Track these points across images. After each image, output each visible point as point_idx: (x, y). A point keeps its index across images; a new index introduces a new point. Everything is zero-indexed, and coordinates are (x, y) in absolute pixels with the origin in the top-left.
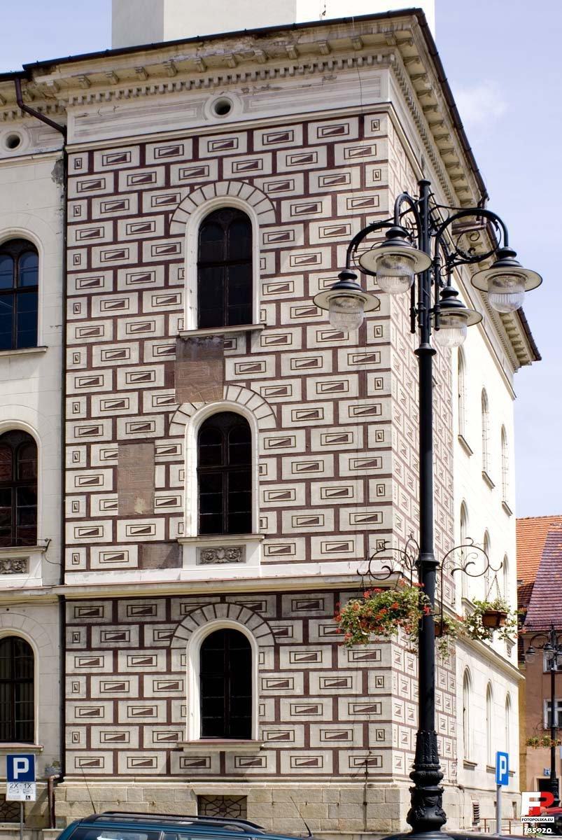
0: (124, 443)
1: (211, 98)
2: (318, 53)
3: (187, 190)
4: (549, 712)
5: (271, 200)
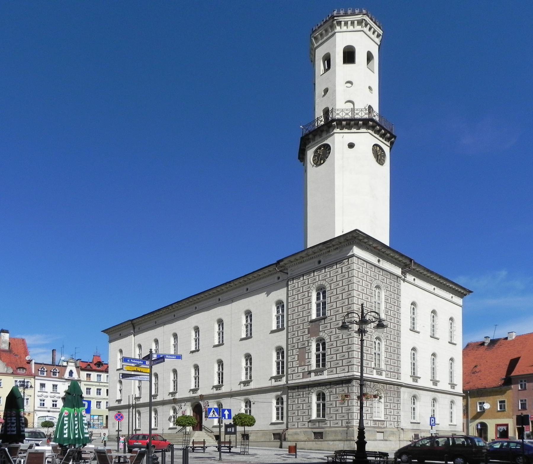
0: (299, 349)
1: (316, 260)
2: (337, 244)
4: (316, 375)
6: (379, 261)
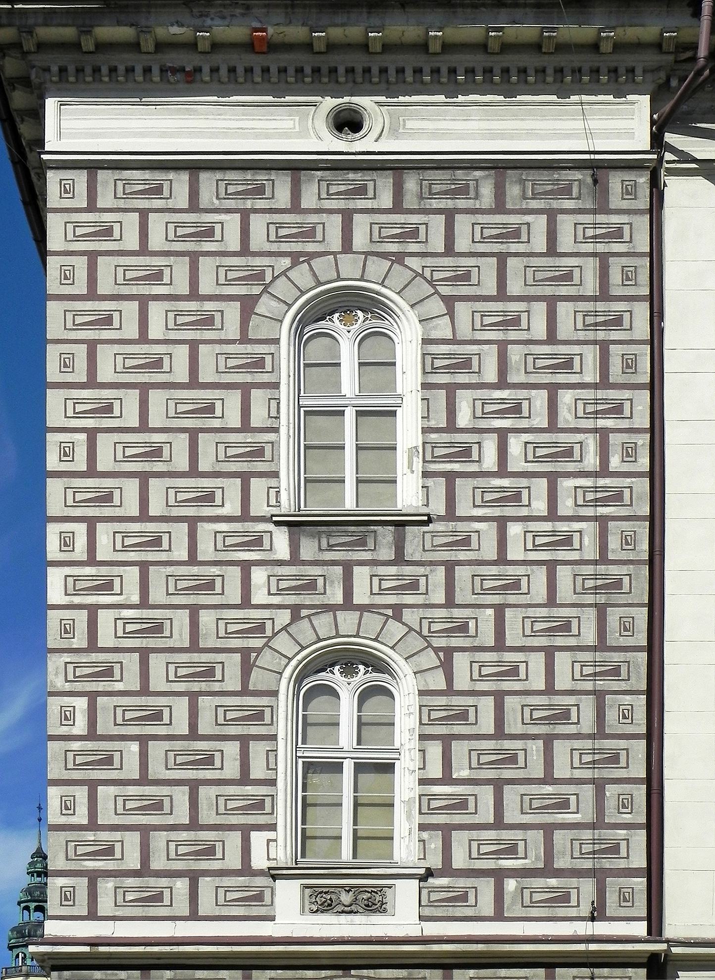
3: (286, 262)
5: (436, 650)
6: (348, 123)
